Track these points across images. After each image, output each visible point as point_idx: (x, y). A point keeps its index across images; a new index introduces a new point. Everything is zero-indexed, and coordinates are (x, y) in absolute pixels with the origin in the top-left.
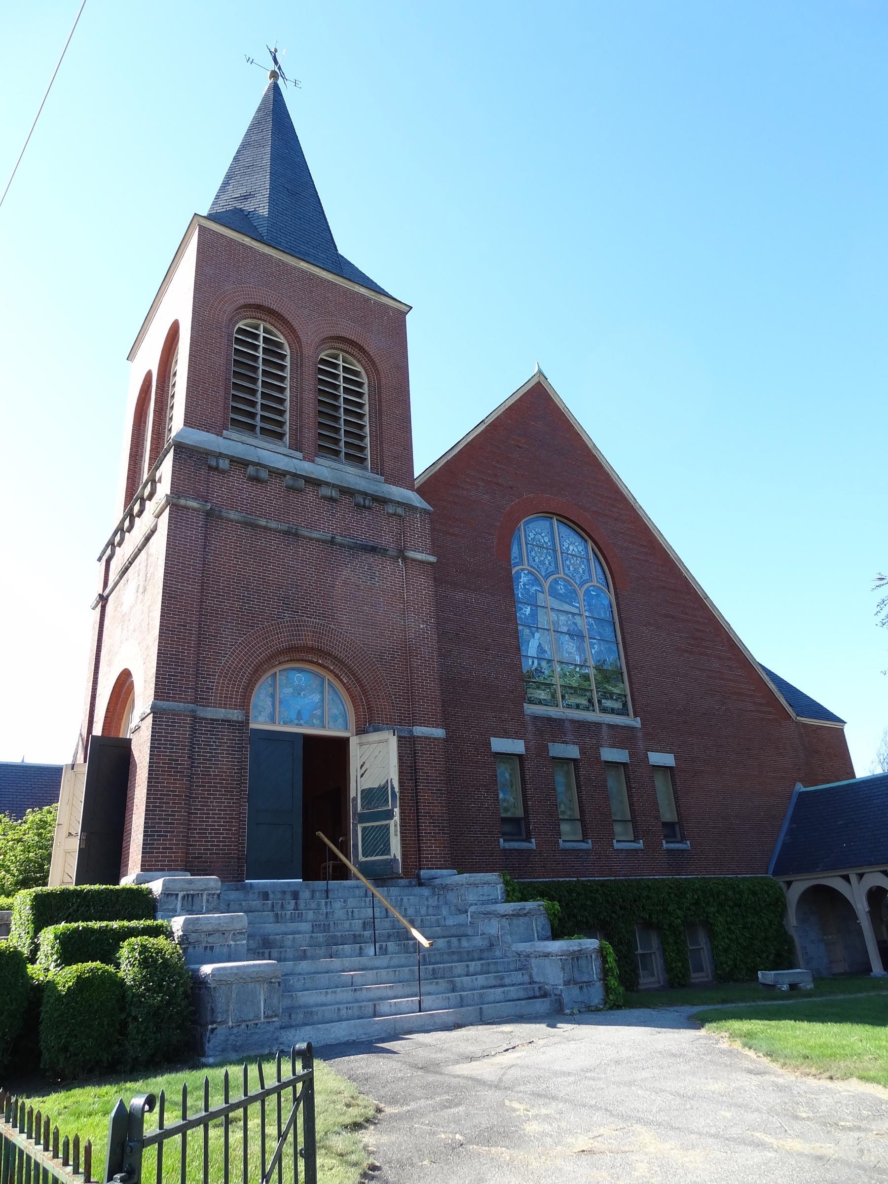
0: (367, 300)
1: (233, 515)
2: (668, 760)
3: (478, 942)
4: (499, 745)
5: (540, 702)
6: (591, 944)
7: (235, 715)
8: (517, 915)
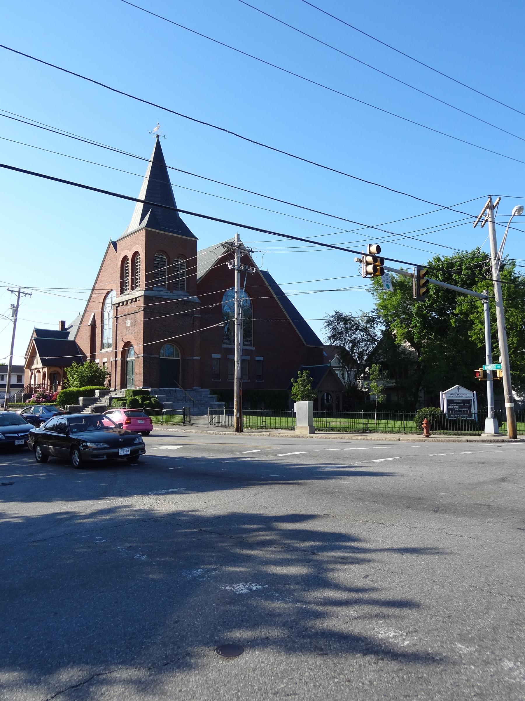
1: (156, 311)
2: (261, 359)
3: (204, 402)
4: (214, 356)
5: (227, 344)
6: (224, 403)
7: (157, 356)
8: (212, 397)
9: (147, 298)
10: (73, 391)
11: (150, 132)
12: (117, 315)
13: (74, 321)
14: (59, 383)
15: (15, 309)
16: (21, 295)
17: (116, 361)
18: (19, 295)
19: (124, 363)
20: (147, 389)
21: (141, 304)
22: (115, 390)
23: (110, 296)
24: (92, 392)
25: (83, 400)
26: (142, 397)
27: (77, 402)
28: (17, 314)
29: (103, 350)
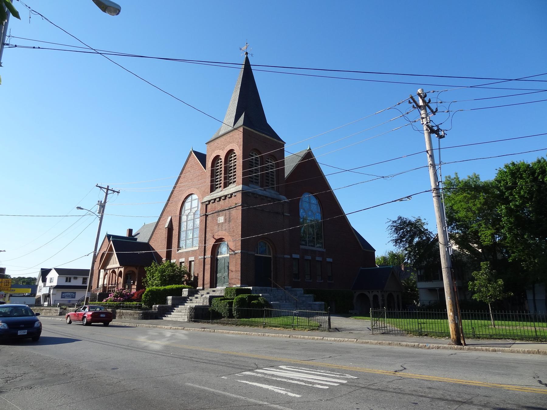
0: (276, 142)
5: (303, 245)
6: (323, 303)
9: (245, 194)
10: (160, 290)
11: (241, 49)
12: (206, 212)
13: (140, 230)
14: (134, 283)
15: (102, 206)
16: (109, 192)
17: (204, 259)
18: (107, 191)
19: (214, 261)
20: (249, 288)
21: (238, 199)
22: (203, 289)
23: (189, 199)
24: (180, 291)
25: (173, 299)
26: (248, 296)
27: (165, 301)
28: (103, 210)
29: (180, 251)
